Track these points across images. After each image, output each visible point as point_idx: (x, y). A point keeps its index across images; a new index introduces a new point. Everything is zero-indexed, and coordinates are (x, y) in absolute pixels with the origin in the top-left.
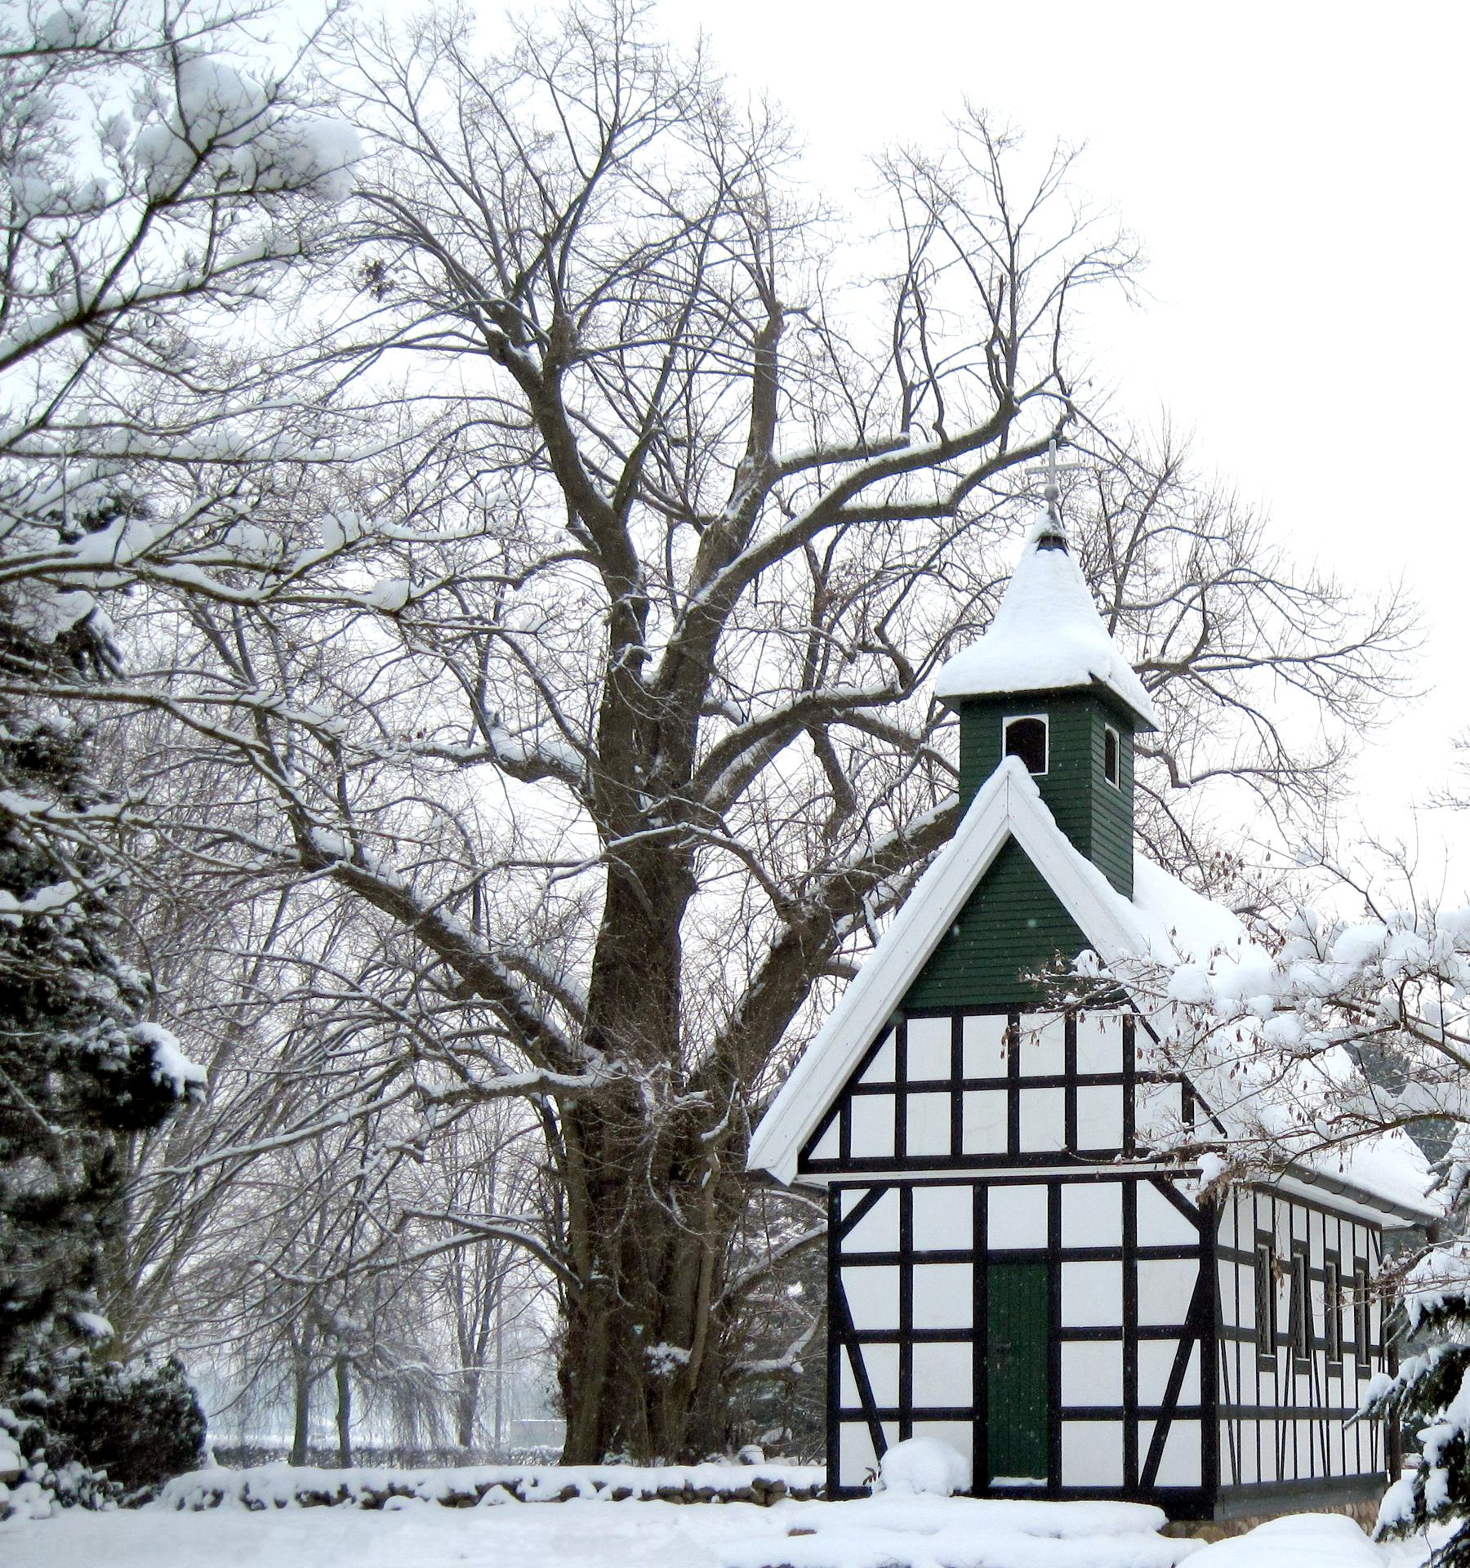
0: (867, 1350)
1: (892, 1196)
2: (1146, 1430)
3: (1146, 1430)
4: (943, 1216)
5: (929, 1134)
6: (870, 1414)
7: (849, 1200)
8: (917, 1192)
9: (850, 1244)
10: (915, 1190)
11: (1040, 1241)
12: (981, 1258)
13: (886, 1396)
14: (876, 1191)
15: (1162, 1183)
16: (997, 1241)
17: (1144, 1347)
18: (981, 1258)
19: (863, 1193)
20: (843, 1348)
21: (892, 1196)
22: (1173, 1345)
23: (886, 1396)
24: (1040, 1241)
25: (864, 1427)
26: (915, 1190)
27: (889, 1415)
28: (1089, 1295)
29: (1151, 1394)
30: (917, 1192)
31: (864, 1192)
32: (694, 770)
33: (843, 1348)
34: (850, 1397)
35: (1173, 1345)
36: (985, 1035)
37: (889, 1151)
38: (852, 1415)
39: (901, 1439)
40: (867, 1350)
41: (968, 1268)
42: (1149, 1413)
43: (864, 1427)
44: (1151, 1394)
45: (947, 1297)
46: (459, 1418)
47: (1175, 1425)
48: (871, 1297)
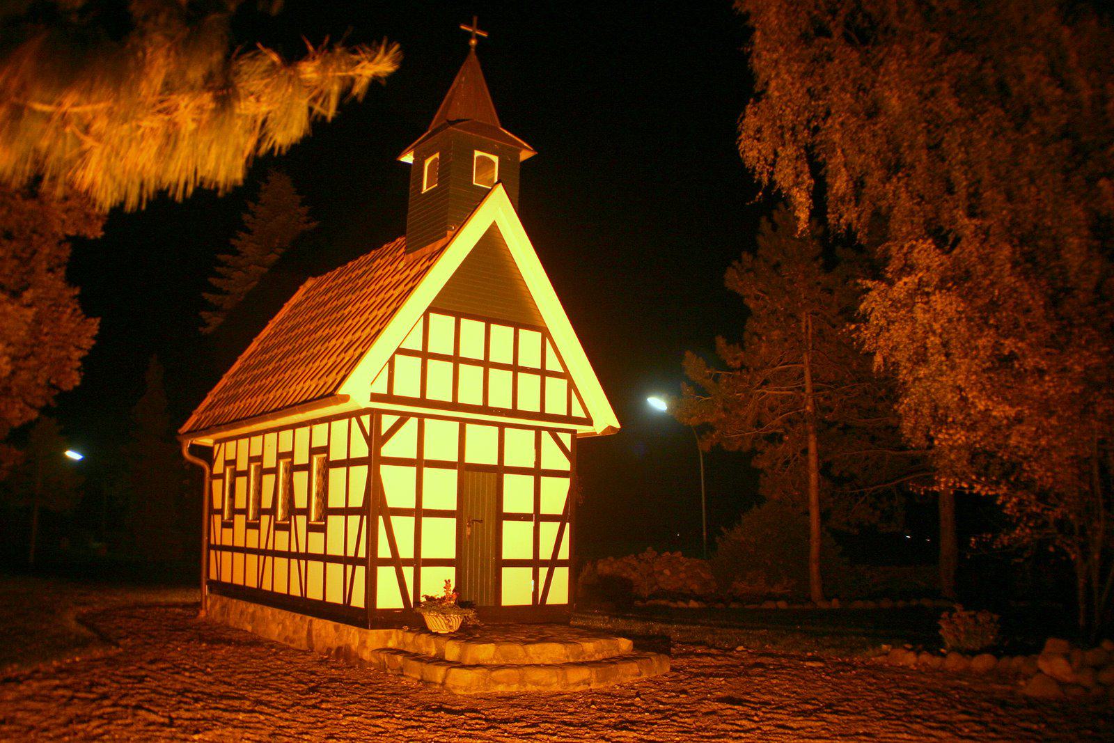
0: (395, 520)
1: (413, 422)
2: (543, 572)
3: (543, 572)
4: (441, 439)
5: (439, 389)
6: (396, 561)
7: (387, 422)
8: (469, 427)
9: (387, 450)
10: (507, 430)
11: (453, 474)
12: (464, 469)
13: (406, 552)
14: (404, 417)
15: (553, 432)
16: (470, 458)
17: (544, 526)
18: (464, 469)
19: (396, 418)
20: (381, 519)
21: (413, 422)
22: (558, 524)
23: (406, 552)
24: (453, 474)
25: (392, 570)
26: (507, 430)
27: (407, 562)
28: (517, 495)
29: (546, 554)
30: (469, 427)
31: (397, 418)
32: (705, 606)
33: (381, 519)
34: (384, 551)
35: (558, 524)
36: (473, 330)
37: (417, 395)
38: (385, 562)
39: (592, 425)
40: (395, 520)
41: (495, 462)
42: (545, 563)
43: (392, 570)
44: (546, 554)
45: (442, 490)
46: (286, 512)
47: (557, 570)
48: (398, 486)
